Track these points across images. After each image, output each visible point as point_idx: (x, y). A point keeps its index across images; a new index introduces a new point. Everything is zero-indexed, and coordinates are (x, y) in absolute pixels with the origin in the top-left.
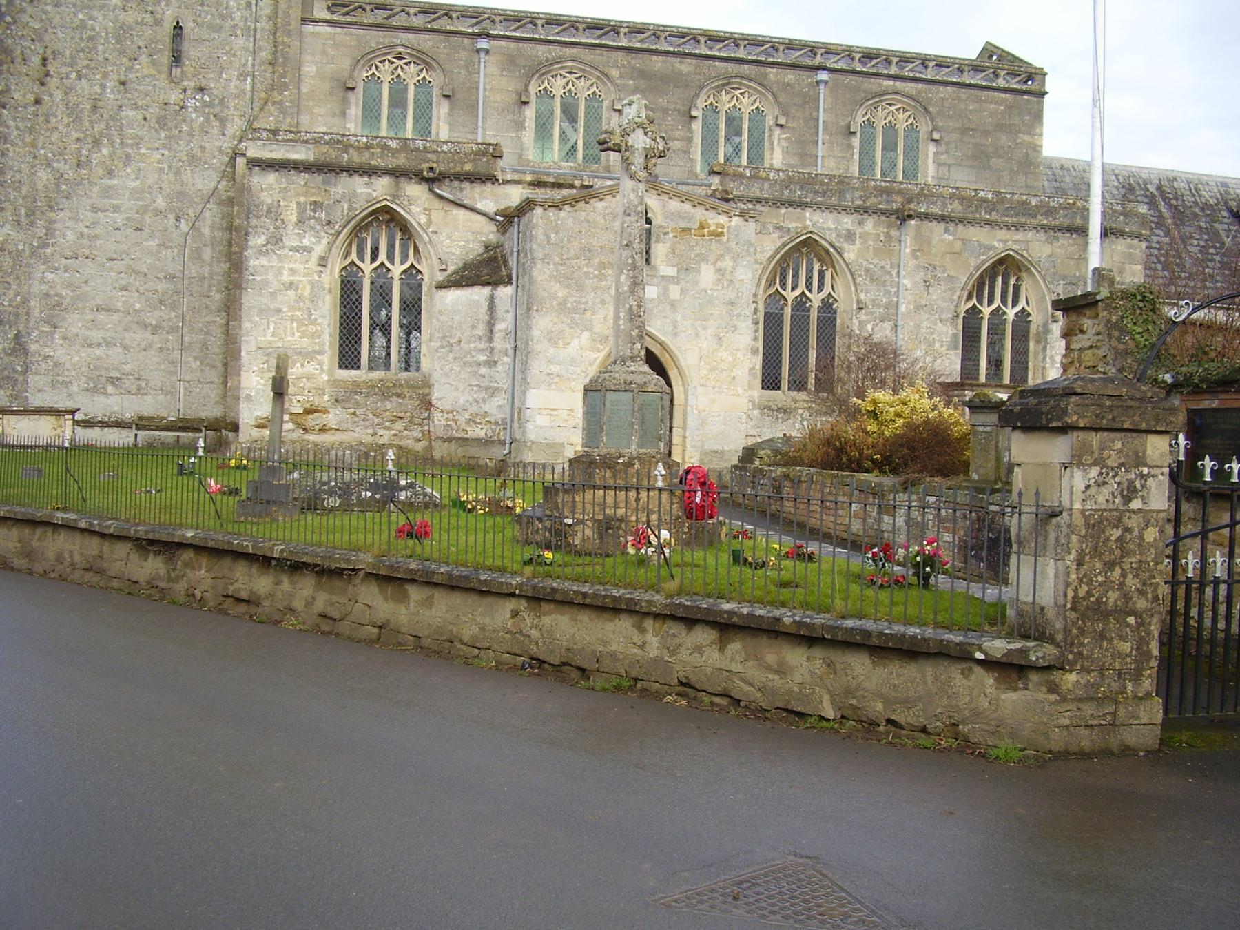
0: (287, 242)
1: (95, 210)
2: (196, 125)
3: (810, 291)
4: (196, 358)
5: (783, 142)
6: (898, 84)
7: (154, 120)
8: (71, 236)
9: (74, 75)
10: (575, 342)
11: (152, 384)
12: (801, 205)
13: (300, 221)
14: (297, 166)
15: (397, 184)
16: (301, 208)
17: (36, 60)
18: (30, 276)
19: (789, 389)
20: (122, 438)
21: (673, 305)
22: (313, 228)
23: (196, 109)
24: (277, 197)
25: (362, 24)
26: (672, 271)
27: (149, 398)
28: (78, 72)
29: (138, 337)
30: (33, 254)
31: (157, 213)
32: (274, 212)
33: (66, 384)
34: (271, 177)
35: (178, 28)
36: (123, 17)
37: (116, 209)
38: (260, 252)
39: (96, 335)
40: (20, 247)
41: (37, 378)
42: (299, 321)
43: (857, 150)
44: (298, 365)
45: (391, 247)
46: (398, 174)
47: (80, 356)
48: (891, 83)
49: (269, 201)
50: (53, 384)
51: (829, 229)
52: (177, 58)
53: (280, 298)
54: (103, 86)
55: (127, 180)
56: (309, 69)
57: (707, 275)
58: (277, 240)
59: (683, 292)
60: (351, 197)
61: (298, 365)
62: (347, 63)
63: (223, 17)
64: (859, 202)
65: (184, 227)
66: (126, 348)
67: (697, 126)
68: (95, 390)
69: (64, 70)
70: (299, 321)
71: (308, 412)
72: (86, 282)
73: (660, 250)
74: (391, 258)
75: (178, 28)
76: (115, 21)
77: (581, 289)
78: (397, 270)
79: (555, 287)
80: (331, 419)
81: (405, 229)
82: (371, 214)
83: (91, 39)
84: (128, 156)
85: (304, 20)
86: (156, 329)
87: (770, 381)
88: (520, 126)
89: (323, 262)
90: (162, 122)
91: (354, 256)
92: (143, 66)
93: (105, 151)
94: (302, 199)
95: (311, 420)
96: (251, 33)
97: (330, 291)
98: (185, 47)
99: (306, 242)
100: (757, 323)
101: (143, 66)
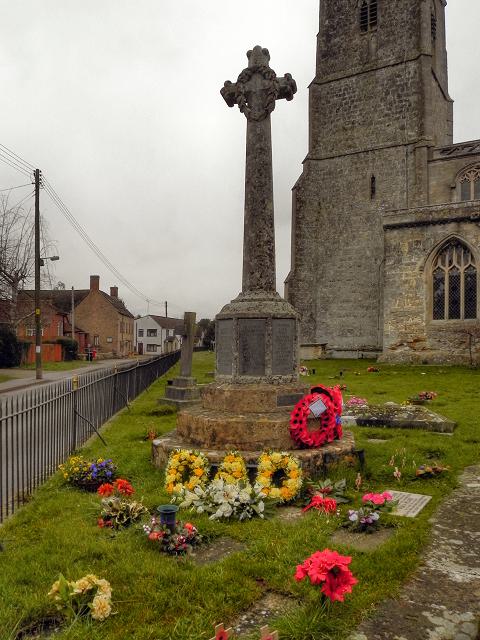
0: (404, 262)
1: (342, 260)
13: (410, 251)
15: (459, 226)
16: (410, 245)
17: (316, 204)
18: (316, 291)
20: (355, 355)
23: (382, 211)
27: (365, 338)
29: (361, 311)
30: (317, 281)
31: (367, 258)
33: (331, 333)
34: (395, 232)
35: (373, 179)
37: (350, 259)
42: (411, 298)
45: (459, 257)
46: (459, 221)
47: (337, 321)
49: (394, 243)
52: (373, 191)
55: (355, 246)
56: (433, 183)
58: (399, 261)
62: (451, 176)
63: (392, 169)
65: (379, 262)
68: (343, 335)
70: (411, 298)
71: (416, 341)
74: (459, 263)
75: (373, 179)
78: (462, 269)
80: (427, 344)
81: (466, 248)
82: (447, 242)
85: (429, 162)
89: (422, 269)
91: (439, 264)
92: (359, 198)
95: (417, 345)
96: (405, 173)
97: (426, 283)
98: (377, 185)
101: (359, 198)
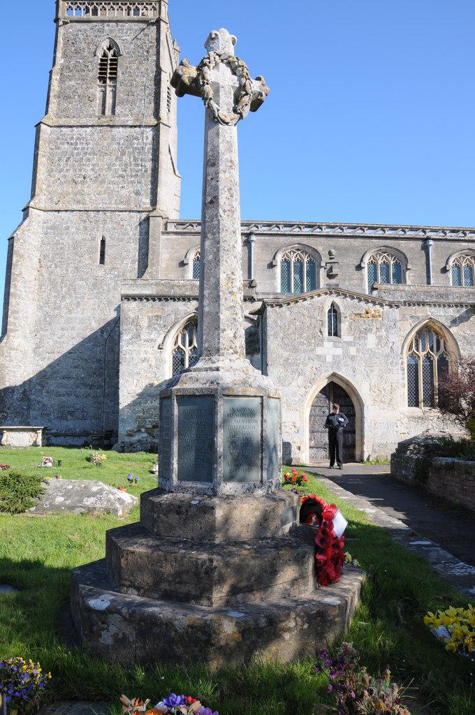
0: (142, 337)
2: (111, 286)
3: (433, 351)
4: (111, 401)
5: (411, 278)
6: (470, 244)
7: (91, 285)
8: (51, 343)
9: (53, 266)
10: (294, 383)
11: (90, 414)
12: (424, 304)
14: (147, 298)
19: (424, 406)
21: (353, 358)
22: (156, 329)
24: (137, 314)
25: (191, 233)
26: (350, 339)
27: (88, 422)
28: (56, 265)
29: (83, 391)
32: (135, 322)
34: (133, 304)
36: (76, 237)
37: (73, 329)
38: (130, 343)
39: (62, 390)
40: (26, 349)
41: (34, 412)
43: (451, 279)
44: (149, 402)
48: (466, 244)
50: (42, 415)
51: (441, 316)
53: (139, 366)
54: (67, 270)
57: (371, 340)
58: (138, 336)
59: (358, 351)
60: (176, 312)
61: (149, 402)
64: (457, 300)
66: (77, 396)
67: (365, 271)
69: (49, 264)
72: (58, 365)
73: (344, 326)
76: (73, 239)
77: (295, 350)
79: (281, 351)
83: (61, 248)
84: (78, 303)
86: (91, 387)
87: (414, 402)
88: (273, 277)
90: (95, 285)
93: (68, 301)
94: (150, 314)
99: (152, 337)
100: (403, 370)
